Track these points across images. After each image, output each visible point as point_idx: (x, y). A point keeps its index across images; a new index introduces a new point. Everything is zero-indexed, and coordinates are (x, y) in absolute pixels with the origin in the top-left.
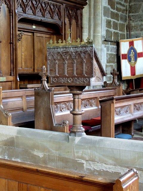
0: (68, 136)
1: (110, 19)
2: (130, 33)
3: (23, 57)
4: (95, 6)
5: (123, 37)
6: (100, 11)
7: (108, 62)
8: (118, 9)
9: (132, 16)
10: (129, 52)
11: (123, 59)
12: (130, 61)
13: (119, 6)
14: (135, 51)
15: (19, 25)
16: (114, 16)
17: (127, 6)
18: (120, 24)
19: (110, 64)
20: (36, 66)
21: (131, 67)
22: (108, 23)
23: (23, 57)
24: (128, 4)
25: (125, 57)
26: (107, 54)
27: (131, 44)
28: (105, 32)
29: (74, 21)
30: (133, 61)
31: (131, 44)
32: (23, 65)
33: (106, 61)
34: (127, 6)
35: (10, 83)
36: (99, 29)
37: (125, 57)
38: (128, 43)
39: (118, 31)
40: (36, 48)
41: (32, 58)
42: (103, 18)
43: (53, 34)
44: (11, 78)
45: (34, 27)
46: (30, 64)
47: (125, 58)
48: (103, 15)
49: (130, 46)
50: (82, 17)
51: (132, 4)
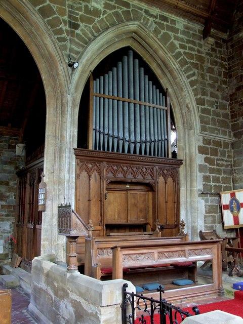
0: (68, 237)
1: (208, 174)
2: (233, 186)
3: (116, 210)
4: (191, 165)
5: (226, 189)
6: (196, 169)
7: (206, 213)
8: (218, 165)
9: (237, 169)
10: (231, 202)
11: (224, 209)
12: (232, 211)
13: (220, 162)
14: (237, 201)
15: (152, 156)
16: (212, 171)
17: (231, 161)
18: (222, 178)
19: (211, 214)
20: (129, 218)
21: (234, 217)
22: (206, 179)
23: (116, 210)
24: (232, 159)
25: (226, 207)
26: (205, 205)
27: (233, 195)
28: (202, 186)
29: (170, 180)
30: (235, 212)
31: (233, 195)
32: (116, 216)
33: (205, 212)
34: (231, 161)
35: (98, 231)
36: (195, 184)
37: (226, 207)
38: (229, 194)
39: (221, 184)
40: (129, 203)
41: (126, 211)
42: (199, 174)
43: (148, 191)
44: (99, 228)
45: (128, 186)
46: (123, 216)
47: (227, 209)
48: (198, 172)
49: (231, 197)
50: (179, 175)
51: (236, 158)
